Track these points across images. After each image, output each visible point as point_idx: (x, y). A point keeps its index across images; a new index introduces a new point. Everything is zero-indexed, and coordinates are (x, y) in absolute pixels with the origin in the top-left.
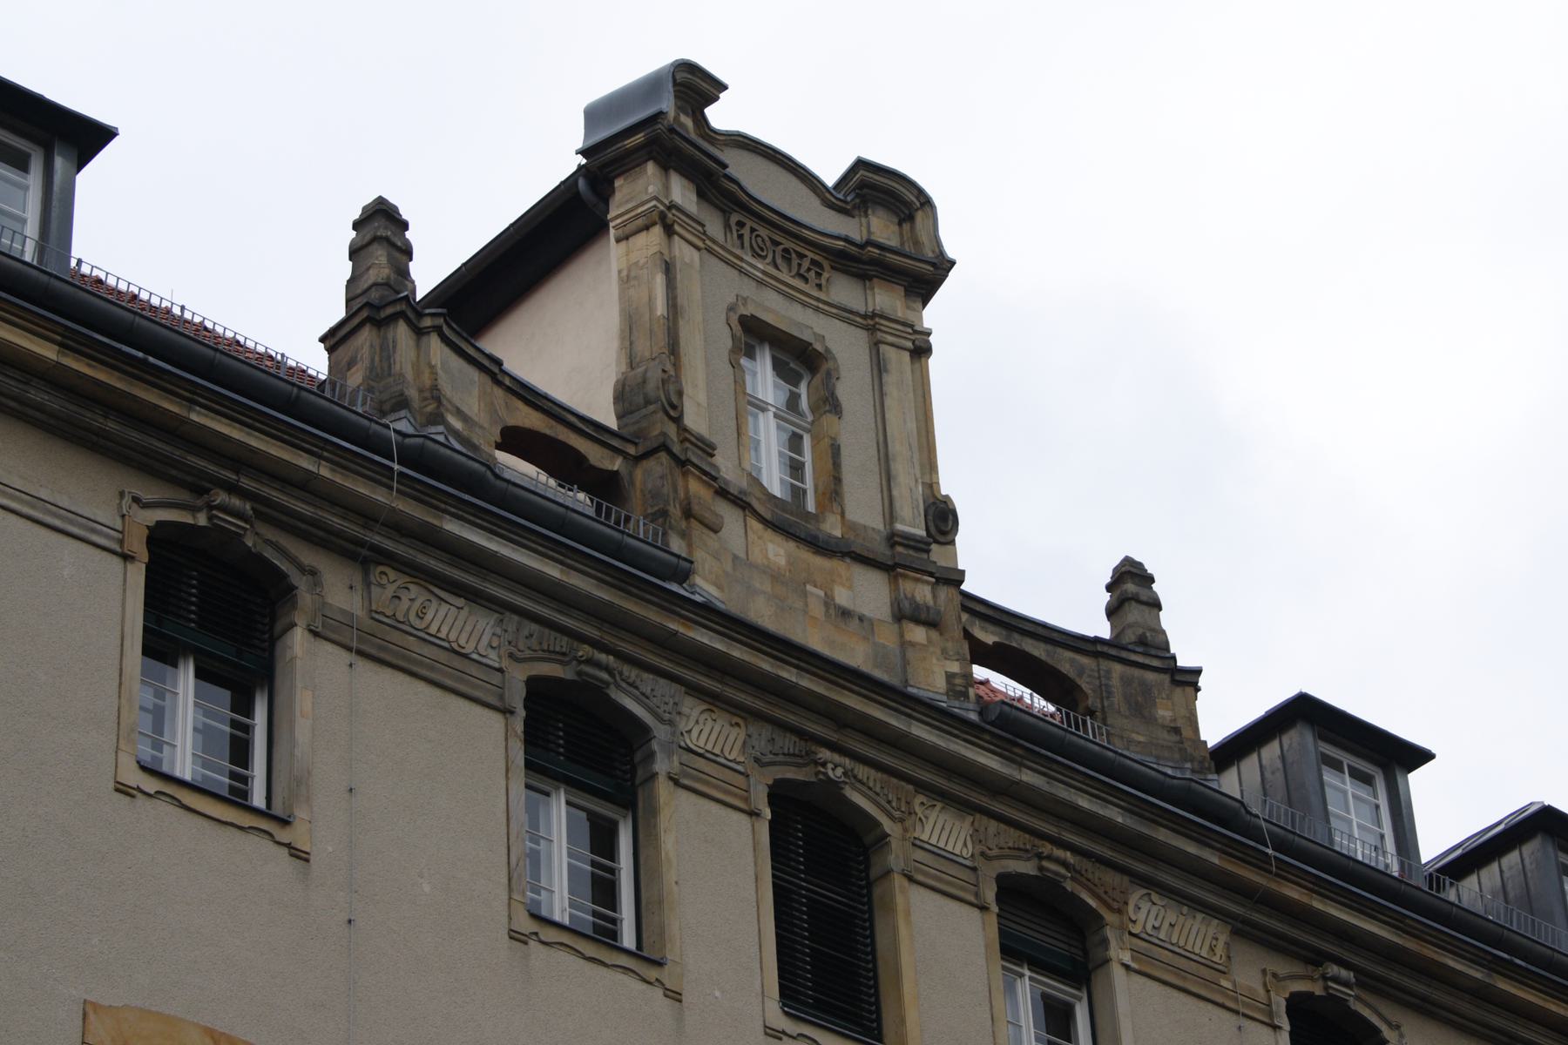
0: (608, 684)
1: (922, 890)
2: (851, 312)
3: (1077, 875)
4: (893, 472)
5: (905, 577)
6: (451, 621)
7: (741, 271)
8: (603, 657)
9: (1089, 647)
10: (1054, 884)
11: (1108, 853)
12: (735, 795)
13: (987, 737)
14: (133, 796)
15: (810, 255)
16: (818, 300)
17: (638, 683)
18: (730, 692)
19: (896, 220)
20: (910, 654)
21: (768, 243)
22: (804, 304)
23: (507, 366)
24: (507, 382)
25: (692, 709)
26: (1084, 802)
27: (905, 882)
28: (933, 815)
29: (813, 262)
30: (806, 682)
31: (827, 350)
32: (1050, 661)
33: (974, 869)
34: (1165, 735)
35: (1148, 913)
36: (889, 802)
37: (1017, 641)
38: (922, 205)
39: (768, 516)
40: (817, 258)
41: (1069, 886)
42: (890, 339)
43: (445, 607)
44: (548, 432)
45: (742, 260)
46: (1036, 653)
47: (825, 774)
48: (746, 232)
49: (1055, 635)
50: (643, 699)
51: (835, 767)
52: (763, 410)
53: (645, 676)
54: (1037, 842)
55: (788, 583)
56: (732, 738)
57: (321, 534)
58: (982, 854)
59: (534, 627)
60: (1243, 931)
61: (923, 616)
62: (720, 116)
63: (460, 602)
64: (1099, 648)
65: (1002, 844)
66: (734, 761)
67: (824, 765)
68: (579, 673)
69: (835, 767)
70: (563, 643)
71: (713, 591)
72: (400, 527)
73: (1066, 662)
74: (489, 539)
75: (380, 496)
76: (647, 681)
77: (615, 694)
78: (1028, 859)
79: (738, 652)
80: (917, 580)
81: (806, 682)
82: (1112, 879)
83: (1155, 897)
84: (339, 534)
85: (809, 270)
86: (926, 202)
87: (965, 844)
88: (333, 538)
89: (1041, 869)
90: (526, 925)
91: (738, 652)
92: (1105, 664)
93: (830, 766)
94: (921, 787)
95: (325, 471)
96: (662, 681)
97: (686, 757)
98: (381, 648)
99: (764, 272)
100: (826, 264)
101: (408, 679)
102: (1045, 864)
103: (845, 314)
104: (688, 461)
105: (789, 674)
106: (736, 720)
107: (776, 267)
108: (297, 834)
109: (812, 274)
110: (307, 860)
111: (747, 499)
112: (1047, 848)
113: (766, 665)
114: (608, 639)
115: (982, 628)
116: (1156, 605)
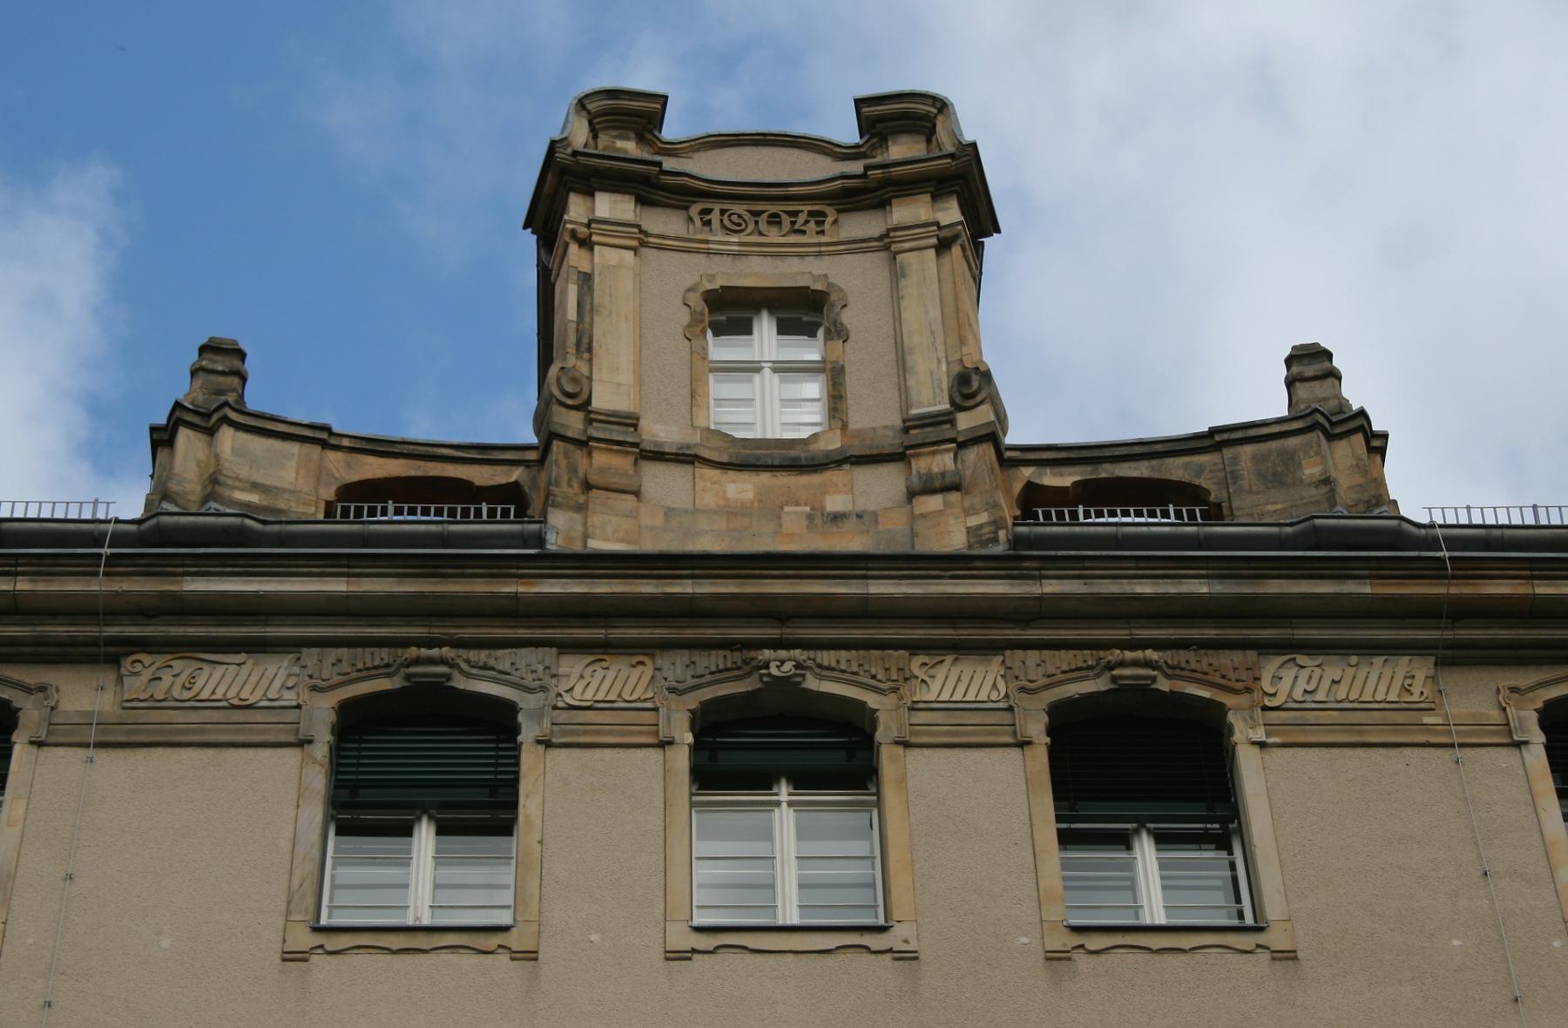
0: (449, 677)
1: (918, 751)
2: (864, 241)
3: (1173, 671)
4: (909, 364)
5: (917, 456)
6: (226, 679)
7: (708, 253)
8: (435, 652)
9: (1207, 443)
10: (1143, 691)
11: (1211, 633)
12: (641, 733)
13: (981, 564)
14: (689, 959)
15: (806, 208)
16: (819, 245)
17: (492, 663)
18: (618, 633)
19: (923, 138)
20: (920, 526)
21: (747, 216)
22: (801, 256)
23: (336, 429)
24: (346, 442)
25: (572, 666)
26: (1145, 588)
27: (900, 750)
28: (941, 672)
29: (811, 214)
30: (707, 588)
31: (830, 285)
32: (1156, 475)
33: (1011, 709)
34: (1313, 491)
35: (1287, 680)
36: (873, 677)
37: (1106, 471)
38: (941, 110)
39: (725, 459)
40: (816, 208)
41: (1164, 685)
42: (907, 245)
43: (221, 669)
44: (413, 473)
45: (707, 242)
46: (1135, 474)
47: (769, 675)
48: (715, 217)
49: (1159, 448)
50: (502, 677)
51: (781, 663)
52: (758, 370)
53: (499, 653)
54: (1102, 654)
55: (771, 510)
56: (633, 679)
57: (52, 649)
58: (1022, 689)
59: (343, 652)
60: (1452, 657)
61: (937, 484)
62: (673, 129)
63: (242, 657)
64: (1218, 438)
65: (1051, 670)
66: (639, 700)
67: (767, 666)
68: (408, 677)
69: (781, 663)
70: (384, 655)
71: (301, 509)
72: (144, 610)
73: (1176, 469)
74: (246, 582)
75: (97, 585)
76: (504, 659)
77: (460, 683)
78: (1097, 676)
79: (603, 587)
80: (934, 453)
81: (707, 588)
82: (1227, 659)
83: (1301, 659)
84: (73, 642)
85: (807, 222)
86: (942, 105)
87: (995, 686)
88: (70, 649)
89: (1114, 679)
90: (304, 939)
91: (603, 587)
92: (1228, 453)
93: (773, 664)
94: (915, 647)
95: (23, 585)
96: (523, 651)
97: (563, 717)
98: (132, 732)
99: (740, 244)
100: (830, 211)
101: (169, 751)
102: (1116, 672)
103: (858, 246)
104: (591, 439)
105: (683, 588)
106: (635, 660)
107: (761, 234)
108: (1276, 938)
109: (812, 224)
110: (1296, 958)
111: (692, 452)
112: (1116, 655)
113: (647, 588)
114: (438, 632)
115: (1054, 475)
116: (1335, 375)
